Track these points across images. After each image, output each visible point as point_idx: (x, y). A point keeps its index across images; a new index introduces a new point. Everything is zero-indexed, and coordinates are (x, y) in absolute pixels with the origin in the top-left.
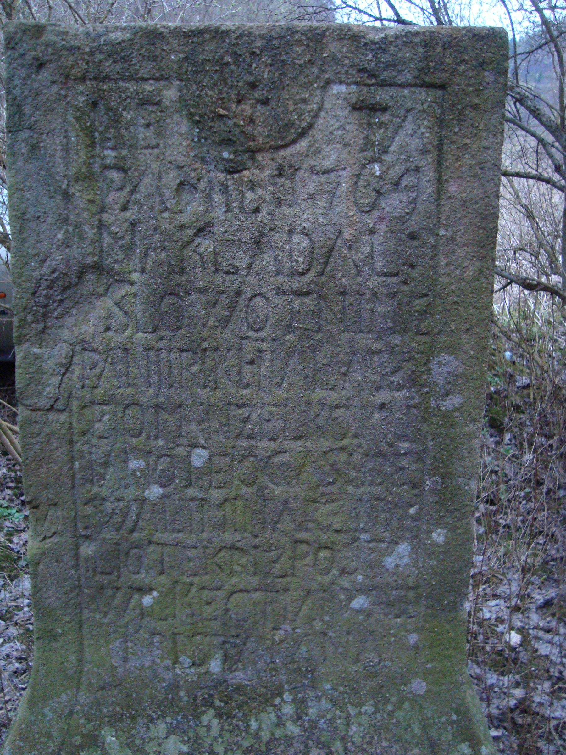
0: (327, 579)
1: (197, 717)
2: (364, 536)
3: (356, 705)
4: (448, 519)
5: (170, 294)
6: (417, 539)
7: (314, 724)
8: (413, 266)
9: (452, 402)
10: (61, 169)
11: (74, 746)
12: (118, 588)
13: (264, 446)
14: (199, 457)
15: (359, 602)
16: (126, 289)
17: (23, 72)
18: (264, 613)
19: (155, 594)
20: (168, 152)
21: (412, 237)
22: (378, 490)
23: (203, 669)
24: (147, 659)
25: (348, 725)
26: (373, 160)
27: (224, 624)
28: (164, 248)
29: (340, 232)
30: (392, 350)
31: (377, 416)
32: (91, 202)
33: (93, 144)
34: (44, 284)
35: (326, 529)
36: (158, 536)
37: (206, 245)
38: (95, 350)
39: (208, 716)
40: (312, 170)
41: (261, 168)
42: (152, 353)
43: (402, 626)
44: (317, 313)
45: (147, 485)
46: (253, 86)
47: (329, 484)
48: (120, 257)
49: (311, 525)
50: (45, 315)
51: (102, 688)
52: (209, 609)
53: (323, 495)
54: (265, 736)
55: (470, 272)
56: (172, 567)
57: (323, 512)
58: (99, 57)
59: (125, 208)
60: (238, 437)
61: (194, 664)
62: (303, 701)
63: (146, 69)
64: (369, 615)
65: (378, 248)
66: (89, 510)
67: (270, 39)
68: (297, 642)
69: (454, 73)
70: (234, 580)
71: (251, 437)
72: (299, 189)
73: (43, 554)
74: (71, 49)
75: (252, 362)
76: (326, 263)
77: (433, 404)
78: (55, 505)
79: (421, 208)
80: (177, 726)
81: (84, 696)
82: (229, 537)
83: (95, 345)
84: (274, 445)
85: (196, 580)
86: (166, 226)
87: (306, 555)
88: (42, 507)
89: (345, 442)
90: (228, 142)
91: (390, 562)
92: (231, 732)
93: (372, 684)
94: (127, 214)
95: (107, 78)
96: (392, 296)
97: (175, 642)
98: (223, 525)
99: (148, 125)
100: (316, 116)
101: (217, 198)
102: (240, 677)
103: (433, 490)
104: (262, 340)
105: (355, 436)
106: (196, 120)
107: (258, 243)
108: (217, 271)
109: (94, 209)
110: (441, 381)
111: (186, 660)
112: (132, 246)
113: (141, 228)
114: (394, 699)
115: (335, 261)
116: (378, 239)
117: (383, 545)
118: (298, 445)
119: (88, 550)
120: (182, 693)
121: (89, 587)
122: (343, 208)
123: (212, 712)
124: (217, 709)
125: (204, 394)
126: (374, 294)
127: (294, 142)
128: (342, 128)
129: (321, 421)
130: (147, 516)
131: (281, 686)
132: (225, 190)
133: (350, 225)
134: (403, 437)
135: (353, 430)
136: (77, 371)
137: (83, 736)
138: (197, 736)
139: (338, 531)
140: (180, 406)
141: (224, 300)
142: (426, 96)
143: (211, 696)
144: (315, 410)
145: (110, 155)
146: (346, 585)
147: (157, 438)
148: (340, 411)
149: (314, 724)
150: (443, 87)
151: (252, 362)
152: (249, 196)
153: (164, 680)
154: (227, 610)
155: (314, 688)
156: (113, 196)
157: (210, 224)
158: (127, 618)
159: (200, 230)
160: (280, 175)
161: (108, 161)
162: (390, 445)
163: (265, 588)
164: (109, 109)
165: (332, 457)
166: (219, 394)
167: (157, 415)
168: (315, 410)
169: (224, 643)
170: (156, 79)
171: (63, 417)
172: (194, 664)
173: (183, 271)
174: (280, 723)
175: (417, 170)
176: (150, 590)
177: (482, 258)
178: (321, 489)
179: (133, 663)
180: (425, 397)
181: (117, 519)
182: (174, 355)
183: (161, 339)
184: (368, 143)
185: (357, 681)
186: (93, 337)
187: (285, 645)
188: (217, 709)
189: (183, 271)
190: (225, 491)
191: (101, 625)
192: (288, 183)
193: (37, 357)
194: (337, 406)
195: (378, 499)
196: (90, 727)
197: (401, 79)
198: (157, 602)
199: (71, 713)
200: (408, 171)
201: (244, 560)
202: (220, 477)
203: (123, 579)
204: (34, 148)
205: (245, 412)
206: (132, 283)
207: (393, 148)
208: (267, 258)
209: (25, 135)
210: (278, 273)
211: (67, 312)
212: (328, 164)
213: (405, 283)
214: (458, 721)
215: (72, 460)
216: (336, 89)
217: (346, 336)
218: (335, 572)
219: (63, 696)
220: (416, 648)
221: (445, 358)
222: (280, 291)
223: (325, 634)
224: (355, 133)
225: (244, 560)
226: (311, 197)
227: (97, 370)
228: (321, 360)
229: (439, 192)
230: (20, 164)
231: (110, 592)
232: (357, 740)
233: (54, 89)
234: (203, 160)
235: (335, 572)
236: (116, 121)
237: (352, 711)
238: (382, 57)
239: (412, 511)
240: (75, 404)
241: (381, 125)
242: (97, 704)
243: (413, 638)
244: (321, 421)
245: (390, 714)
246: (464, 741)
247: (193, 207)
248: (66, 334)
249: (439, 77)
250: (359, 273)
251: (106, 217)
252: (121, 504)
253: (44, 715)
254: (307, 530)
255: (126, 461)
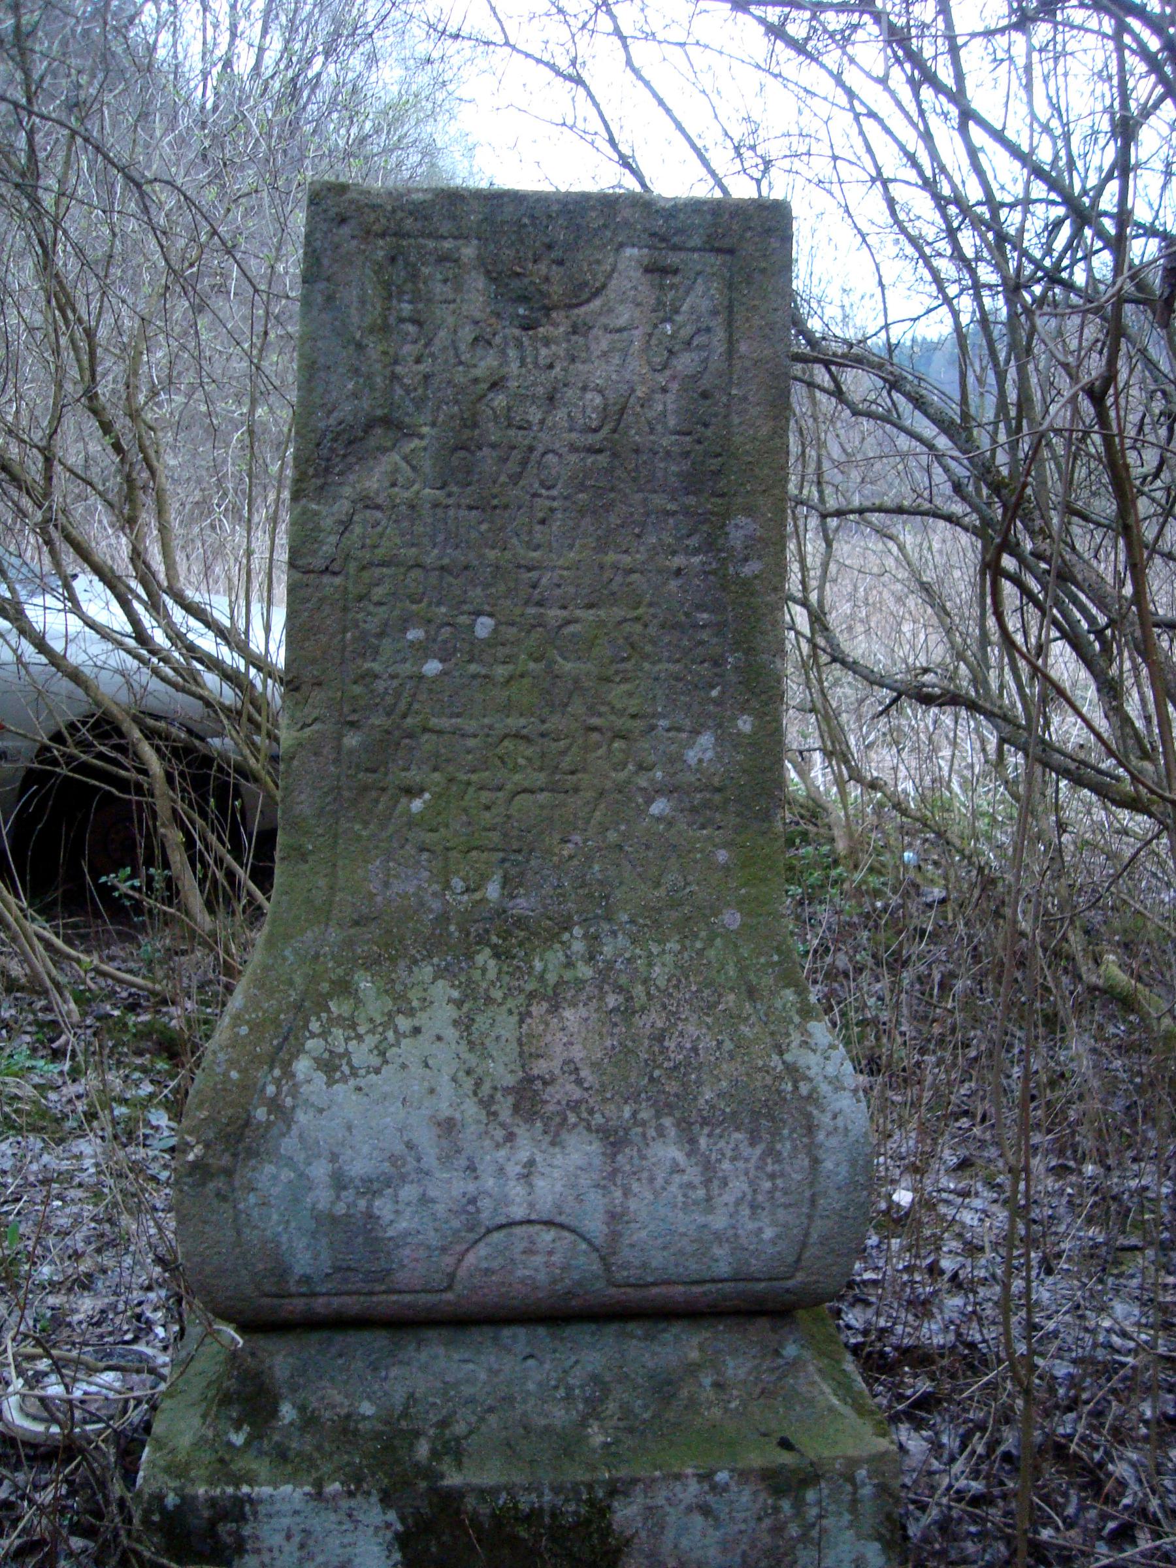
0: (622, 776)
1: (470, 957)
2: (663, 723)
3: (659, 942)
4: (755, 704)
5: (461, 447)
6: (720, 726)
7: (610, 965)
8: (706, 425)
9: (748, 570)
10: (355, 320)
11: (321, 995)
12: (383, 790)
13: (554, 614)
14: (484, 627)
15: (659, 807)
16: (416, 443)
17: (324, 226)
18: (551, 819)
19: (427, 796)
20: (465, 307)
21: (705, 395)
22: (675, 668)
23: (477, 896)
24: (411, 884)
25: (650, 965)
26: (664, 320)
27: (505, 835)
28: (457, 402)
29: (633, 390)
30: (687, 512)
31: (673, 585)
32: (385, 353)
33: (390, 297)
34: (329, 436)
35: (620, 713)
36: (434, 722)
37: (500, 400)
38: (378, 507)
39: (484, 957)
40: (606, 328)
41: (556, 325)
42: (439, 511)
43: (709, 838)
44: (609, 471)
45: (426, 658)
46: (549, 247)
47: (623, 660)
48: (411, 410)
49: (603, 709)
50: (327, 470)
51: (356, 923)
52: (487, 815)
53: (617, 672)
54: (552, 978)
55: (764, 431)
56: (448, 761)
57: (616, 693)
58: (400, 214)
59: (418, 361)
60: (526, 603)
61: (468, 890)
62: (596, 938)
63: (445, 228)
64: (670, 824)
65: (670, 407)
66: (357, 689)
67: (566, 205)
68: (589, 859)
69: (742, 237)
70: (517, 777)
71: (540, 604)
72: (593, 346)
73: (300, 744)
74: (374, 207)
75: (543, 522)
76: (619, 421)
77: (731, 570)
78: (319, 684)
79: (712, 367)
80: (446, 969)
81: (334, 934)
82: (514, 722)
83: (379, 501)
84: (565, 613)
85: (474, 777)
86: (459, 379)
87: (598, 746)
88: (304, 688)
89: (640, 611)
90: (524, 299)
91: (692, 756)
92: (511, 974)
93: (674, 915)
94: (421, 367)
95: (408, 235)
96: (687, 454)
97: (447, 859)
98: (507, 708)
99: (445, 281)
100: (609, 276)
101: (512, 353)
102: (522, 905)
103: (736, 668)
104: (554, 499)
105: (650, 605)
106: (493, 277)
107: (551, 399)
108: (509, 426)
109: (387, 360)
110: (738, 545)
111: (458, 884)
112: (424, 399)
113: (435, 381)
114: (703, 934)
115: (628, 418)
116: (670, 398)
117: (684, 735)
118: (590, 615)
119: (352, 740)
120: (452, 928)
121: (350, 789)
122: (637, 366)
123: (487, 951)
124: (494, 947)
125: (491, 554)
126: (668, 453)
127: (588, 301)
128: (635, 288)
129: (614, 587)
130: (423, 697)
131: (570, 917)
132: (519, 345)
133: (643, 383)
134: (700, 607)
135: (648, 598)
136: (358, 530)
137: (332, 982)
138: (470, 980)
139: (634, 716)
140: (466, 568)
141: (516, 455)
142: (716, 260)
143: (487, 931)
144: (608, 574)
145: (406, 308)
146: (644, 784)
147: (439, 604)
148: (635, 577)
149: (610, 965)
150: (731, 252)
151: (543, 522)
152: (544, 352)
153: (431, 911)
154: (509, 817)
155: (609, 920)
156: (407, 348)
157: (503, 378)
158: (391, 829)
159: (494, 385)
160: (574, 333)
161: (405, 314)
162: (687, 614)
163: (552, 788)
164: (407, 264)
165: (627, 628)
166: (508, 555)
167: (441, 578)
168: (608, 574)
169: (503, 861)
170: (455, 238)
171: (337, 580)
172: (468, 890)
173: (475, 425)
174: (569, 965)
175: (708, 330)
176: (422, 791)
177: (775, 418)
178: (615, 667)
179: (397, 887)
180: (723, 562)
181: (389, 700)
182: (463, 513)
183: (449, 495)
184: (660, 303)
185: (659, 911)
186: (377, 493)
187: (575, 862)
188: (494, 947)
189: (475, 425)
190: (511, 667)
191: (359, 838)
192: (581, 340)
193: (316, 513)
194: (632, 571)
195: (678, 679)
196: (340, 971)
197: (691, 244)
198: (428, 806)
199: (316, 956)
200: (699, 331)
201: (529, 752)
202: (507, 650)
203: (390, 777)
204: (330, 298)
205: (534, 575)
206: (421, 437)
207: (685, 308)
208: (560, 414)
209: (322, 285)
210: (571, 430)
211: (350, 467)
212: (622, 322)
213: (699, 442)
214: (780, 963)
215: (344, 630)
216: (629, 252)
217: (640, 496)
218: (631, 767)
219: (309, 934)
220: (726, 868)
221: (741, 520)
222: (573, 448)
223: (620, 847)
224: (646, 293)
225: (529, 752)
226: (605, 354)
227: (379, 529)
228: (614, 520)
229: (731, 352)
230: (315, 313)
231: (374, 794)
232: (662, 983)
233: (354, 243)
234: (498, 315)
235: (631, 767)
236: (414, 276)
237: (655, 950)
238: (672, 223)
239: (714, 693)
240: (352, 567)
241: (672, 286)
242: (350, 943)
243: (722, 856)
244: (614, 587)
245: (700, 953)
246: (787, 986)
247: (486, 363)
248: (347, 491)
249: (726, 243)
250: (652, 431)
251: (398, 369)
252: (395, 683)
253: (284, 959)
254: (600, 715)
255: (404, 630)
